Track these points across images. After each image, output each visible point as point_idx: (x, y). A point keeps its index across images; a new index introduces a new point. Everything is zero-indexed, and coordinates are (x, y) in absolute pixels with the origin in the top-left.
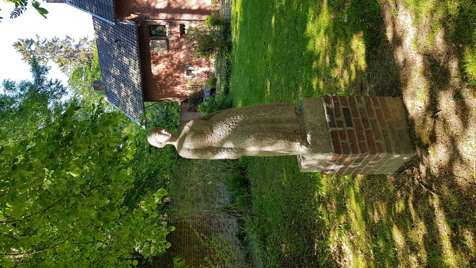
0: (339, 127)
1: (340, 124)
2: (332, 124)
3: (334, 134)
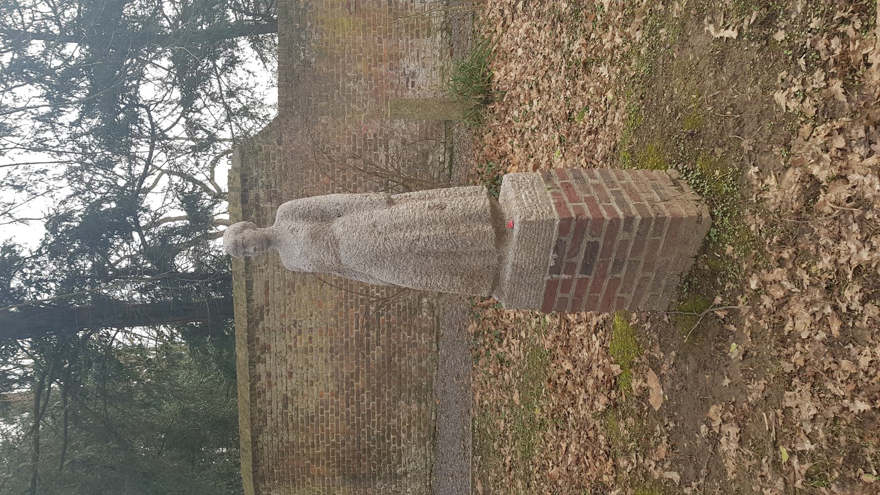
2: (555, 270)
3: (552, 286)
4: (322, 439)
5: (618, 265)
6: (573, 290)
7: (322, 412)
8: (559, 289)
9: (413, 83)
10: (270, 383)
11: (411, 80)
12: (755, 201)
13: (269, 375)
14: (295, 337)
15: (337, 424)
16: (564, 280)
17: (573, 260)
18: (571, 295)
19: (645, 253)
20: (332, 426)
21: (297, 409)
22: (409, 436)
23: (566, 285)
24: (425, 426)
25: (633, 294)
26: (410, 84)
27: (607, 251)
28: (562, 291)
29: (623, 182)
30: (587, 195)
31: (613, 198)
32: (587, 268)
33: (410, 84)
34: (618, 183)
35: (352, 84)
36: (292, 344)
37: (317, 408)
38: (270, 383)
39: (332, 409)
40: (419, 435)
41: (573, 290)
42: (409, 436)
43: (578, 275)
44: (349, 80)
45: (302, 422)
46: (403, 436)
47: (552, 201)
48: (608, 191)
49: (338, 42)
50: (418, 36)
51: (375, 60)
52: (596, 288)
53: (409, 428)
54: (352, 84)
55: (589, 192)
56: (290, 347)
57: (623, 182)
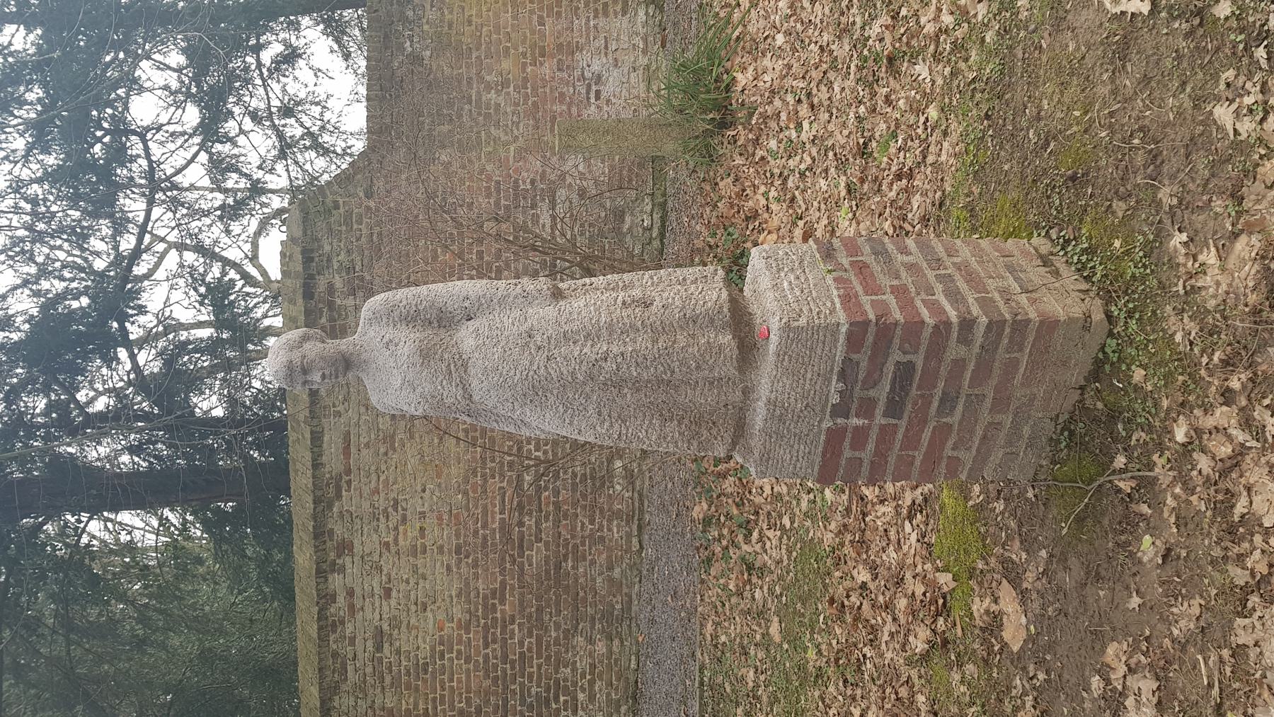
0: (857, 416)
1: (867, 408)
3: (835, 437)
4: (442, 703)
5: (948, 402)
6: (871, 446)
7: (442, 657)
8: (847, 443)
9: (598, 93)
10: (352, 607)
11: (594, 88)
12: (1182, 292)
13: (351, 593)
14: (396, 528)
15: (468, 677)
16: (856, 428)
17: (872, 393)
18: (867, 454)
19: (994, 382)
20: (459, 681)
21: (398, 652)
22: (592, 698)
23: (860, 437)
24: (618, 680)
25: (974, 452)
26: (592, 95)
27: (929, 379)
28: (853, 448)
29: (955, 260)
30: (895, 282)
31: (939, 288)
32: (894, 408)
33: (592, 95)
34: (948, 262)
35: (493, 94)
36: (390, 539)
37: (433, 649)
38: (352, 607)
39: (459, 652)
40: (608, 695)
41: (871, 446)
42: (592, 698)
43: (880, 419)
44: (488, 88)
45: (408, 673)
46: (581, 696)
47: (835, 292)
48: (930, 275)
49: (470, 23)
50: (606, 14)
51: (533, 54)
52: (911, 442)
53: (592, 683)
54: (493, 94)
55: (898, 277)
56: (387, 544)
57: (955, 260)
